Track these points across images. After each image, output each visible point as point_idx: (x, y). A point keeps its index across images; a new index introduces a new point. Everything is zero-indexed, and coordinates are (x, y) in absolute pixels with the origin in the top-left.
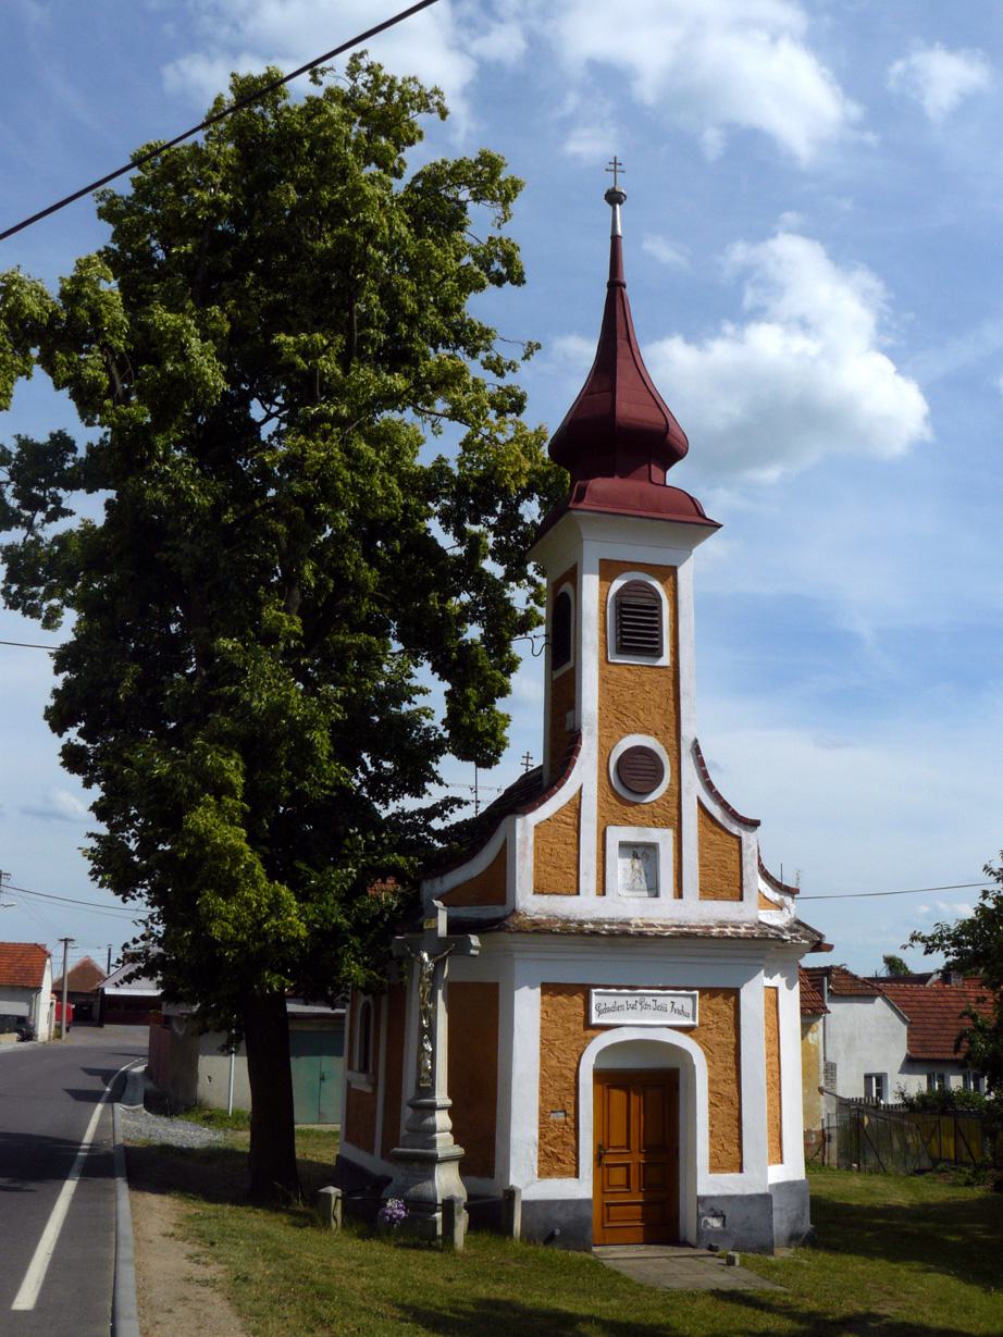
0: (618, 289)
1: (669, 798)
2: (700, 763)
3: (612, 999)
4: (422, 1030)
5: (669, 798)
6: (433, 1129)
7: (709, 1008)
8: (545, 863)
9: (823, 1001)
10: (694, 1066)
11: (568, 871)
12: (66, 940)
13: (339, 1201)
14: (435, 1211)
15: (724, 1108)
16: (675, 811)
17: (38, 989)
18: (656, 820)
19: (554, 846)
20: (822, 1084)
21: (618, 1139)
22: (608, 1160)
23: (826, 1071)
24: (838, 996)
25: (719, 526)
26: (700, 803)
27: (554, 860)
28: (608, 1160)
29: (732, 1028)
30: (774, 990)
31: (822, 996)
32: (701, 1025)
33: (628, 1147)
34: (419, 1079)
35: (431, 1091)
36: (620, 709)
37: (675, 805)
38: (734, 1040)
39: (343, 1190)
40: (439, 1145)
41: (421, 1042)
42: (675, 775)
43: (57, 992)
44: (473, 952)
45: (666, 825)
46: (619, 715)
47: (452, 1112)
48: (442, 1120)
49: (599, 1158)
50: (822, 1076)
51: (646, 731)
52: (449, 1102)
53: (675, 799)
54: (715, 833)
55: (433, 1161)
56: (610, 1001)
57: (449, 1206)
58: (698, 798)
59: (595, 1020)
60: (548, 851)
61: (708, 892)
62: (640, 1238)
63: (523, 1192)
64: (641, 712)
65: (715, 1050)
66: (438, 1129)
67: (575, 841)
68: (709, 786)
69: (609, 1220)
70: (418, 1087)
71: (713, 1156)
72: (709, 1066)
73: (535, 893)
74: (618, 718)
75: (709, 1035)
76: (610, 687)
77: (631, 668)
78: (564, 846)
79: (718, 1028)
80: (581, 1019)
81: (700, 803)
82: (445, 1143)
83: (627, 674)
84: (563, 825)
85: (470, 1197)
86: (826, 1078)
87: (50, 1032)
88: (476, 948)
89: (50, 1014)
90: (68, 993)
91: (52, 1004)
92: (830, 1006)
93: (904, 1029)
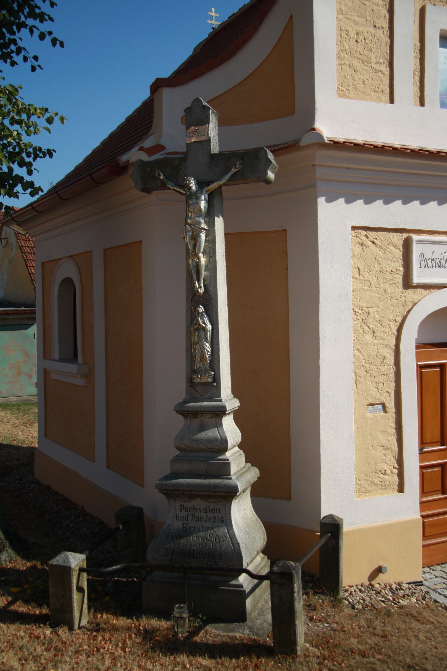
11: (378, 67)
19: (361, 29)
56: (428, 250)
59: (416, 280)
60: (353, 34)
80: (399, 278)
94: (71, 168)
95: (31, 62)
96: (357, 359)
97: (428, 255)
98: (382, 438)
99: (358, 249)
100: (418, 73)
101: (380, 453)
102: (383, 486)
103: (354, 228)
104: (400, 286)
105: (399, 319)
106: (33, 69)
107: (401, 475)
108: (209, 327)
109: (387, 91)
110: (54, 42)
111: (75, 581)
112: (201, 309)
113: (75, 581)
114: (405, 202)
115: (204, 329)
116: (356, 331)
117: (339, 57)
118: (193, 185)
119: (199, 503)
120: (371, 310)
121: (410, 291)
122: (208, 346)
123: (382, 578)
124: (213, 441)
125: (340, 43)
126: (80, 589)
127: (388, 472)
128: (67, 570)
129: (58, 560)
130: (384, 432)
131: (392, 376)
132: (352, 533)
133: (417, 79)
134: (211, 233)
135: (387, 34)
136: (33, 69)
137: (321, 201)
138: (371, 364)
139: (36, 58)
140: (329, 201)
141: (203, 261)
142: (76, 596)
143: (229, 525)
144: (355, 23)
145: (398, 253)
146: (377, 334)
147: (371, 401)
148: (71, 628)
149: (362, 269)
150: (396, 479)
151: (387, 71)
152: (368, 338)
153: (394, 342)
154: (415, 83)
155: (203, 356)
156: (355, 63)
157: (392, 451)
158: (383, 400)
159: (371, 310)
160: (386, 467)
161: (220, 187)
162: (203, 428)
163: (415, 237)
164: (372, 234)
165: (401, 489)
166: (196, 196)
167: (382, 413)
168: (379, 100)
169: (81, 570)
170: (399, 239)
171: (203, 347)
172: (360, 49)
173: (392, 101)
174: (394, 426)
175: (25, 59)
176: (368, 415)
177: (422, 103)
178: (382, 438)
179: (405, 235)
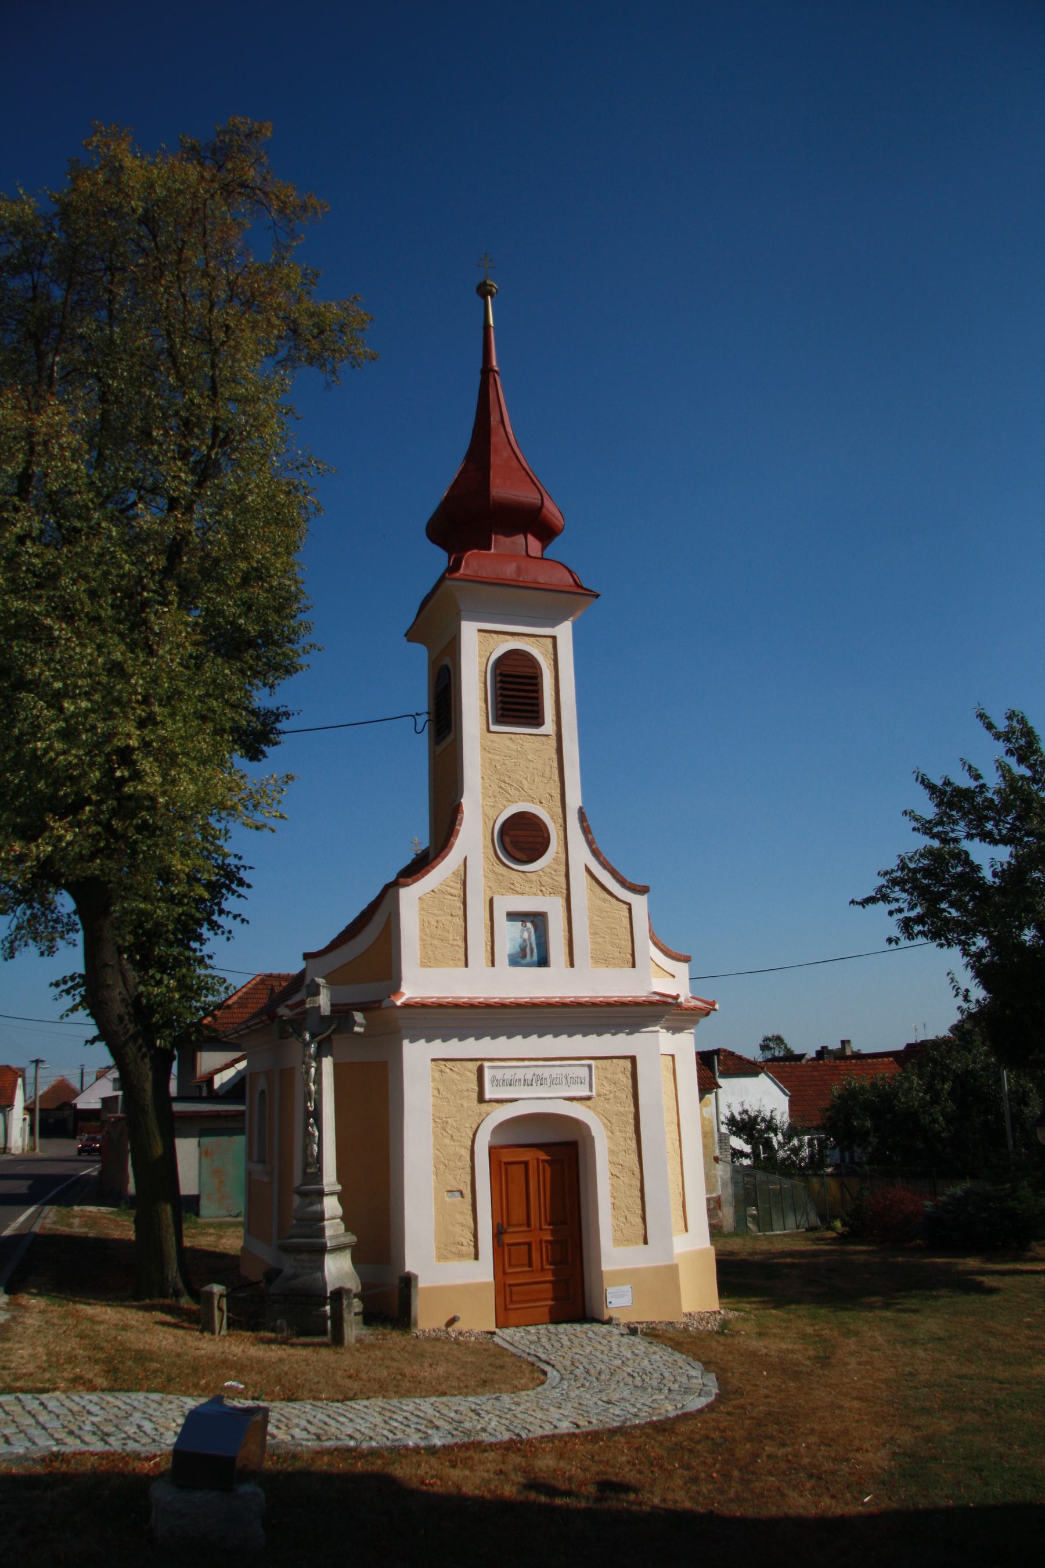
0: (491, 374)
1: (557, 867)
2: (586, 830)
3: (512, 1071)
4: (308, 1114)
5: (557, 867)
6: (320, 1217)
7: (606, 1078)
8: (432, 937)
9: (714, 1077)
10: (592, 1138)
11: (455, 943)
12: (37, 1062)
13: (224, 1300)
14: (325, 1305)
15: (626, 1180)
16: (563, 880)
17: (11, 1105)
18: (544, 889)
19: (440, 918)
20: (717, 1153)
21: (518, 1214)
22: (508, 1239)
23: (720, 1141)
24: (727, 1074)
25: (597, 596)
26: (588, 870)
27: (439, 932)
28: (508, 1239)
29: (630, 1096)
30: (626, 907)
31: (713, 1073)
32: (599, 1095)
33: (529, 1225)
34: (306, 1164)
35: (318, 1175)
36: (502, 778)
37: (563, 873)
38: (632, 1109)
39: (227, 1287)
40: (328, 1232)
41: (307, 1124)
42: (562, 843)
43: (29, 1109)
44: (357, 1029)
45: (554, 892)
46: (503, 785)
47: (342, 1198)
48: (331, 1206)
49: (498, 1234)
50: (717, 1146)
51: (532, 800)
52: (338, 1188)
53: (563, 868)
54: (604, 900)
55: (321, 1250)
56: (499, 1074)
57: (339, 1294)
58: (586, 866)
59: (488, 1095)
60: (434, 923)
61: (601, 959)
62: (547, 1318)
63: (420, 1279)
64: (524, 781)
65: (613, 1121)
66: (327, 1216)
67: (461, 913)
68: (596, 853)
69: (512, 1301)
70: (305, 1172)
71: (617, 1229)
72: (608, 1137)
73: (423, 965)
74: (501, 787)
75: (608, 1106)
76: (491, 756)
77: (513, 736)
78: (450, 918)
79: (616, 1097)
80: (475, 1095)
81: (588, 870)
82: (333, 1229)
83: (509, 743)
84: (449, 897)
85: (364, 1285)
86: (721, 1148)
87: (23, 1145)
88: (360, 1025)
89: (23, 1130)
90: (41, 1110)
91: (24, 1119)
92: (721, 1081)
93: (787, 1099)
94: (343, 928)
95: (226, 935)
96: (436, 1157)
97: (499, 1077)
98: (459, 1217)
99: (437, 1075)
100: (489, 943)
101: (458, 1229)
102: (461, 1256)
103: (433, 1060)
104: (476, 1102)
105: (475, 1127)
106: (228, 939)
107: (476, 1247)
108: (317, 1133)
109: (463, 958)
110: (243, 920)
111: (216, 1302)
112: (312, 1120)
113: (216, 1302)
114: (478, 1038)
115: (313, 1135)
116: (436, 1135)
117: (422, 940)
118: (307, 1036)
119: (304, 1256)
120: (449, 1120)
121: (485, 1105)
122: (315, 1147)
123: (457, 1326)
124: (315, 1213)
125: (422, 930)
126: (220, 1309)
127: (465, 1243)
128: (211, 1294)
129: (207, 1288)
130: (462, 1213)
131: (469, 1170)
132: (423, 1289)
133: (489, 948)
134: (319, 1070)
135: (462, 919)
136: (228, 939)
137: (406, 1043)
138: (449, 1160)
139: (230, 932)
140: (412, 1041)
141: (313, 1088)
142: (217, 1313)
143: (323, 1271)
144: (435, 915)
145: (474, 1077)
146: (455, 1138)
147: (449, 1189)
148: (213, 1333)
149: (441, 1089)
150: (472, 1250)
151: (462, 945)
152: (447, 1141)
153: (470, 1143)
154: (486, 950)
155: (312, 1154)
156: (435, 942)
157: (469, 1228)
158: (461, 1188)
159: (449, 1120)
160: (463, 1240)
161: (329, 1036)
162: (311, 1204)
163: (486, 1064)
164: (449, 1064)
165: (476, 1257)
166: (307, 1045)
167: (460, 1198)
168: (457, 966)
169: (221, 1296)
170: (473, 1066)
171: (312, 1148)
172: (439, 932)
173: (466, 965)
174: (470, 1208)
175: (223, 933)
176: (447, 1199)
177: (493, 965)
178: (459, 1217)
179: (479, 1063)
